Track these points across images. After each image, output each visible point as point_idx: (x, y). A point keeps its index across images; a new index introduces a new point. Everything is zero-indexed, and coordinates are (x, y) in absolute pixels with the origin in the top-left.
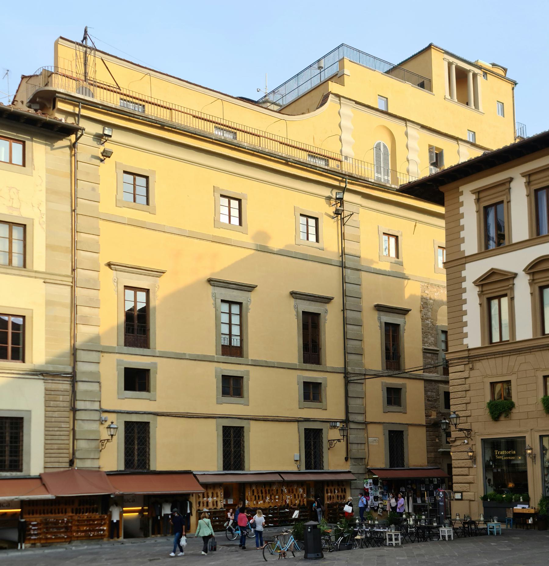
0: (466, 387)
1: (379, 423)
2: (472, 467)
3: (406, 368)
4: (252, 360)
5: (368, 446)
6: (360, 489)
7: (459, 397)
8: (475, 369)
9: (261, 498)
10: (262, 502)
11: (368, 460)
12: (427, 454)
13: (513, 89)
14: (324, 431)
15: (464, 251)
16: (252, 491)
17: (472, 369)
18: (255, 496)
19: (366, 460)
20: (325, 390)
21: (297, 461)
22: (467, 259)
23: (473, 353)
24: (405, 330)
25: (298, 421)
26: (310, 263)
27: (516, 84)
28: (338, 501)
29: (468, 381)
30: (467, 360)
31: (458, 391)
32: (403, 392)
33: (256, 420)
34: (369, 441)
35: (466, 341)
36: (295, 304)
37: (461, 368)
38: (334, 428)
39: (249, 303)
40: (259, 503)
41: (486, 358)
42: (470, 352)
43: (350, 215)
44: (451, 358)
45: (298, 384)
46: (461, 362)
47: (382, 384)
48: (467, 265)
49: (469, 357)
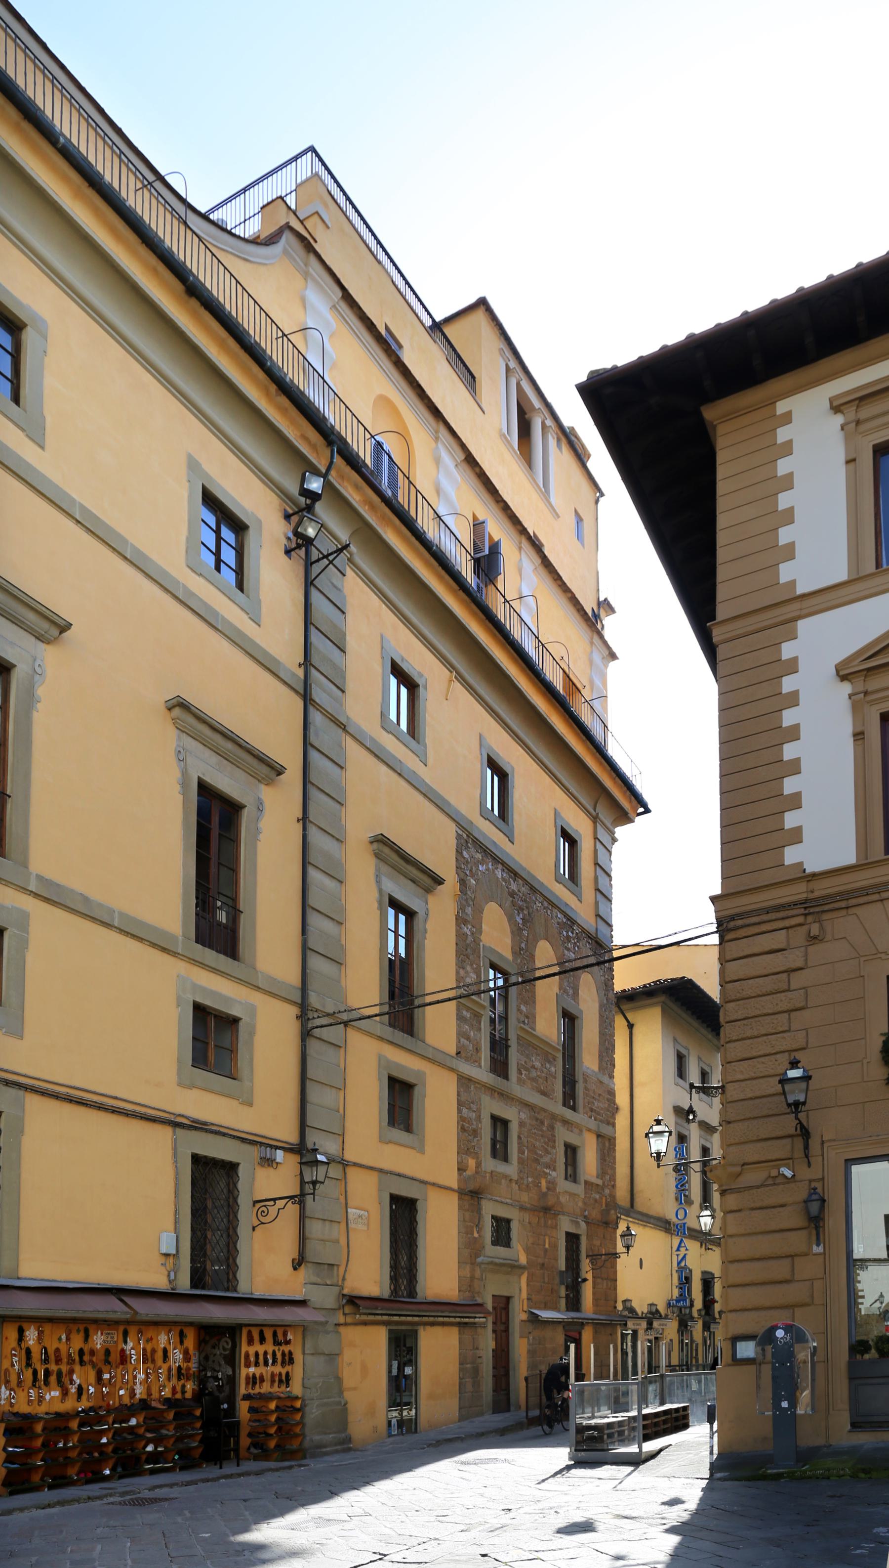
0: (796, 998)
1: (371, 1168)
2: (806, 1255)
3: (538, 964)
4: (40, 878)
5: (348, 1232)
6: (324, 1354)
7: (763, 1032)
8: (829, 937)
9: (53, 1379)
10: (56, 1393)
11: (346, 1271)
12: (459, 1267)
13: (597, 502)
14: (241, 1171)
15: (793, 583)
16: (23, 1352)
17: (813, 939)
18: (35, 1373)
19: (342, 1270)
20: (250, 1043)
21: (167, 1255)
22: (807, 603)
23: (821, 889)
24: (426, 931)
25: (175, 1124)
26: (225, 644)
27: (602, 495)
28: (272, 1390)
29: (797, 980)
30: (802, 911)
31: (759, 1013)
32: (417, 1091)
33: (44, 1093)
34: (350, 1216)
35: (791, 855)
36: (178, 746)
37: (778, 939)
38: (269, 1165)
39: (37, 677)
40: (48, 1397)
41: (876, 897)
42: (815, 885)
43: (335, 552)
44: (738, 910)
45: (178, 1006)
46: (783, 919)
47: (380, 1061)
48: (802, 625)
49: (806, 901)
